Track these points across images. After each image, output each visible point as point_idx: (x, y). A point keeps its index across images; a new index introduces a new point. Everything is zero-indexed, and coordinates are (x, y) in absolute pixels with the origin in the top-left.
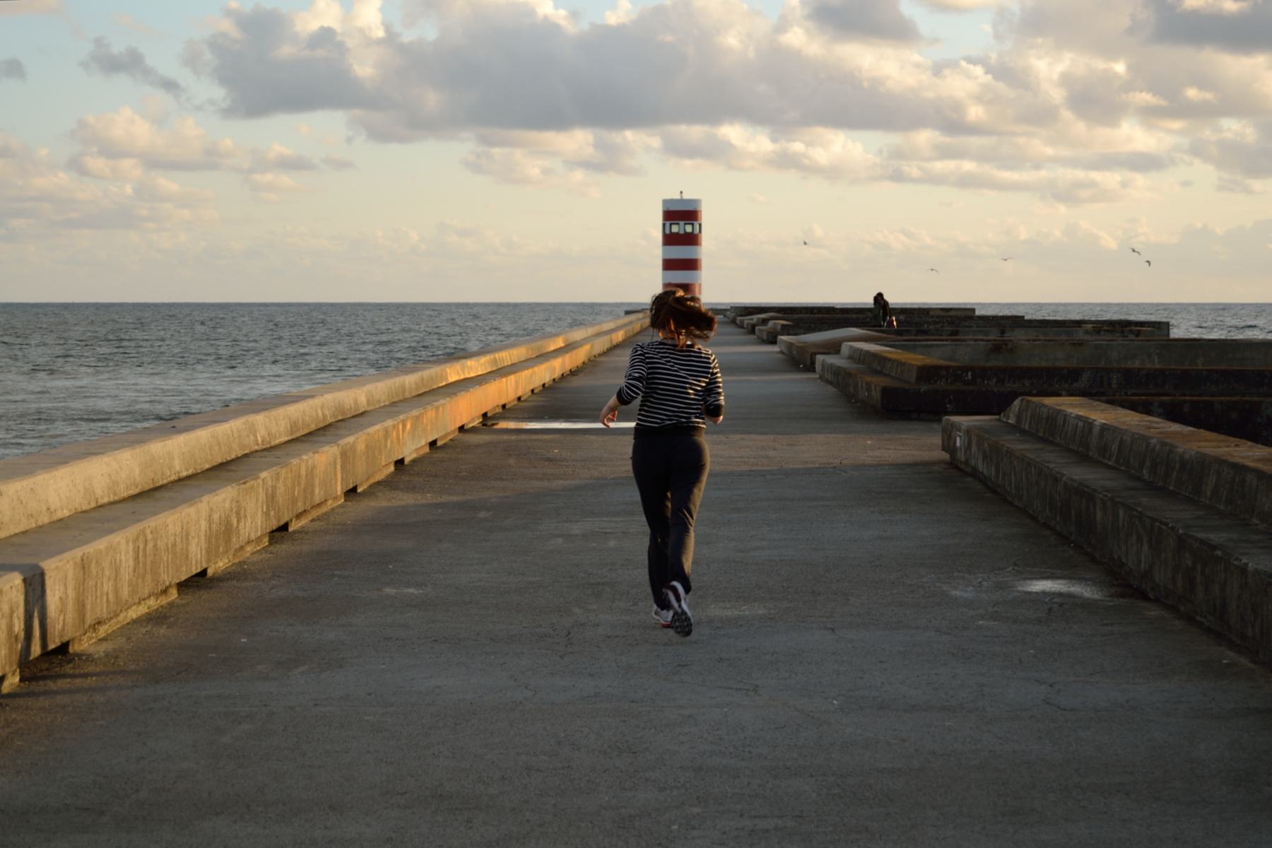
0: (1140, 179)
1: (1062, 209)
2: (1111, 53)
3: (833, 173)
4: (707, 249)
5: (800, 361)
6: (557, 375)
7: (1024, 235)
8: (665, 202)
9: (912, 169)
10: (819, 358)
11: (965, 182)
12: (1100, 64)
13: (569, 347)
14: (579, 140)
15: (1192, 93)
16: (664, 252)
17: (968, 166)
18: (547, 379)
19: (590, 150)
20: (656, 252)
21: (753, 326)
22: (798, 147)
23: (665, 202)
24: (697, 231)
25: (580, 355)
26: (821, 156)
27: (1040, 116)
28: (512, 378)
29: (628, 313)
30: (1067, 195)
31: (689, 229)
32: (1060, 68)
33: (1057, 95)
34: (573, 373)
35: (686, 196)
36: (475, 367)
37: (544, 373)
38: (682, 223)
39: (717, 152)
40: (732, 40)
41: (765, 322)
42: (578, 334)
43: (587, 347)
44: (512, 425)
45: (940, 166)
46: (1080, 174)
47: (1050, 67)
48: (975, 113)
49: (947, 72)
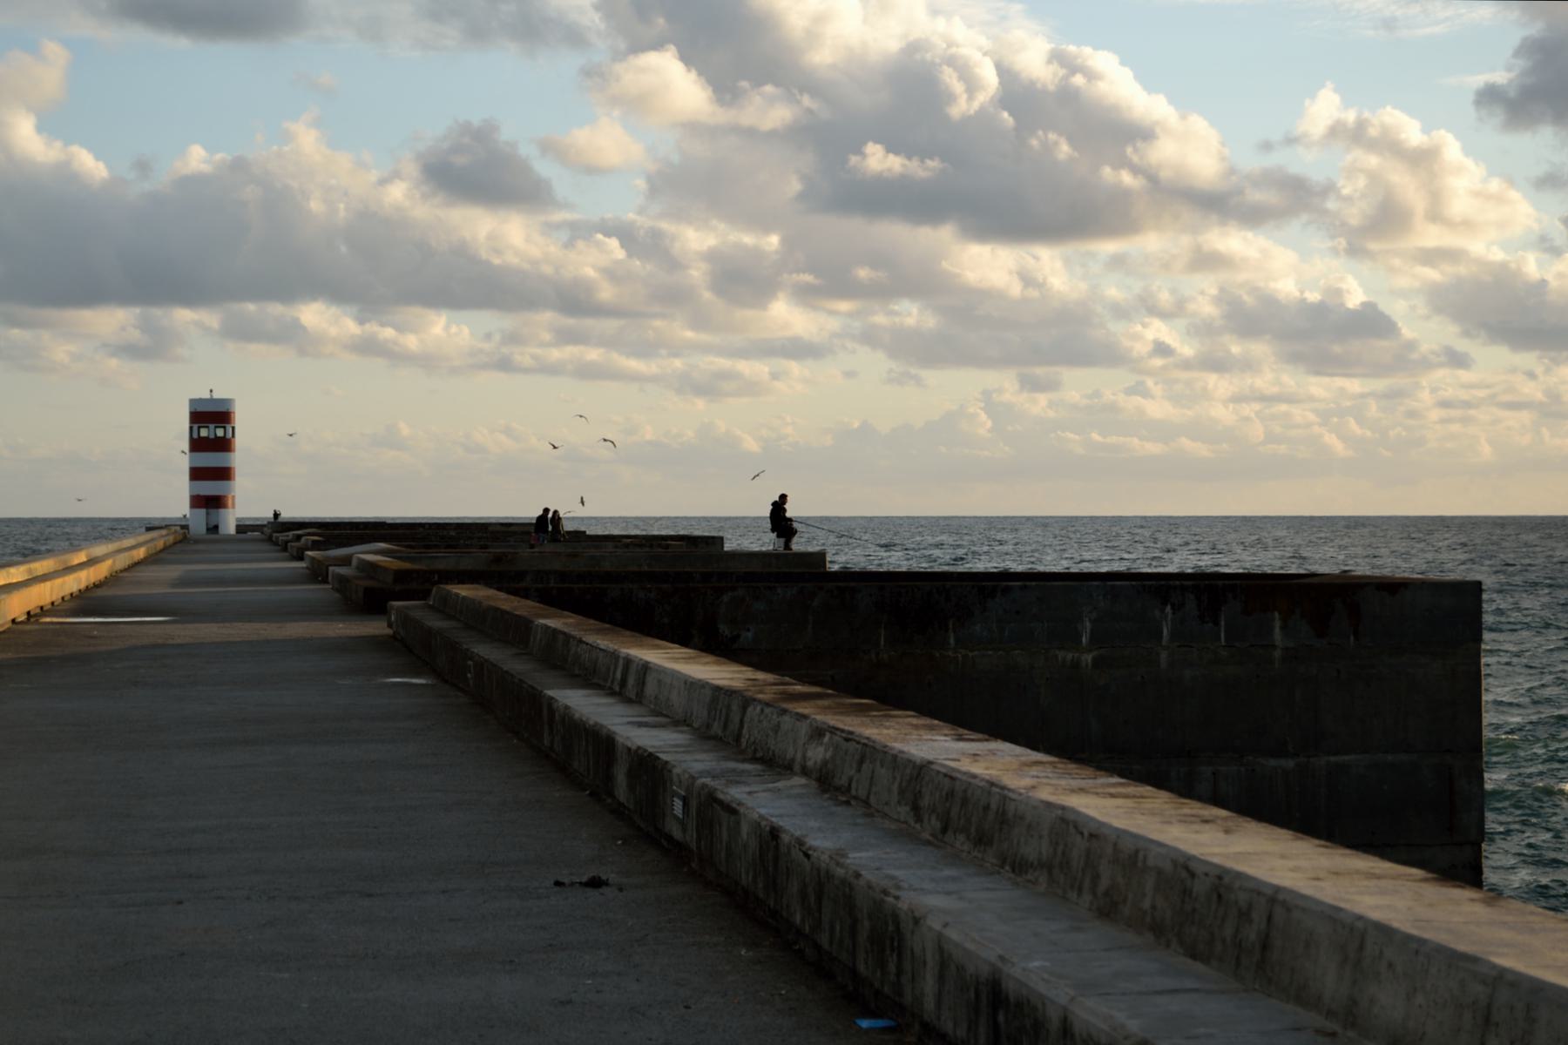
0: (794, 367)
1: (700, 403)
2: (763, 223)
3: (427, 361)
4: (238, 460)
5: (318, 574)
6: (82, 586)
7: (649, 434)
8: (192, 401)
11: (587, 372)
12: (748, 239)
13: (91, 562)
14: (113, 320)
15: (863, 273)
16: (191, 460)
17: (593, 355)
20: (182, 461)
23: (192, 401)
24: (229, 435)
26: (411, 342)
27: (673, 298)
28: (48, 584)
30: (709, 388)
31: (220, 433)
33: (697, 274)
34: (97, 586)
35: (216, 396)
38: (212, 426)
39: (291, 335)
40: (315, 205)
41: (298, 538)
42: (99, 550)
43: (109, 562)
45: (556, 354)
46: (724, 363)
47: (697, 239)
48: (606, 293)
49: (580, 244)
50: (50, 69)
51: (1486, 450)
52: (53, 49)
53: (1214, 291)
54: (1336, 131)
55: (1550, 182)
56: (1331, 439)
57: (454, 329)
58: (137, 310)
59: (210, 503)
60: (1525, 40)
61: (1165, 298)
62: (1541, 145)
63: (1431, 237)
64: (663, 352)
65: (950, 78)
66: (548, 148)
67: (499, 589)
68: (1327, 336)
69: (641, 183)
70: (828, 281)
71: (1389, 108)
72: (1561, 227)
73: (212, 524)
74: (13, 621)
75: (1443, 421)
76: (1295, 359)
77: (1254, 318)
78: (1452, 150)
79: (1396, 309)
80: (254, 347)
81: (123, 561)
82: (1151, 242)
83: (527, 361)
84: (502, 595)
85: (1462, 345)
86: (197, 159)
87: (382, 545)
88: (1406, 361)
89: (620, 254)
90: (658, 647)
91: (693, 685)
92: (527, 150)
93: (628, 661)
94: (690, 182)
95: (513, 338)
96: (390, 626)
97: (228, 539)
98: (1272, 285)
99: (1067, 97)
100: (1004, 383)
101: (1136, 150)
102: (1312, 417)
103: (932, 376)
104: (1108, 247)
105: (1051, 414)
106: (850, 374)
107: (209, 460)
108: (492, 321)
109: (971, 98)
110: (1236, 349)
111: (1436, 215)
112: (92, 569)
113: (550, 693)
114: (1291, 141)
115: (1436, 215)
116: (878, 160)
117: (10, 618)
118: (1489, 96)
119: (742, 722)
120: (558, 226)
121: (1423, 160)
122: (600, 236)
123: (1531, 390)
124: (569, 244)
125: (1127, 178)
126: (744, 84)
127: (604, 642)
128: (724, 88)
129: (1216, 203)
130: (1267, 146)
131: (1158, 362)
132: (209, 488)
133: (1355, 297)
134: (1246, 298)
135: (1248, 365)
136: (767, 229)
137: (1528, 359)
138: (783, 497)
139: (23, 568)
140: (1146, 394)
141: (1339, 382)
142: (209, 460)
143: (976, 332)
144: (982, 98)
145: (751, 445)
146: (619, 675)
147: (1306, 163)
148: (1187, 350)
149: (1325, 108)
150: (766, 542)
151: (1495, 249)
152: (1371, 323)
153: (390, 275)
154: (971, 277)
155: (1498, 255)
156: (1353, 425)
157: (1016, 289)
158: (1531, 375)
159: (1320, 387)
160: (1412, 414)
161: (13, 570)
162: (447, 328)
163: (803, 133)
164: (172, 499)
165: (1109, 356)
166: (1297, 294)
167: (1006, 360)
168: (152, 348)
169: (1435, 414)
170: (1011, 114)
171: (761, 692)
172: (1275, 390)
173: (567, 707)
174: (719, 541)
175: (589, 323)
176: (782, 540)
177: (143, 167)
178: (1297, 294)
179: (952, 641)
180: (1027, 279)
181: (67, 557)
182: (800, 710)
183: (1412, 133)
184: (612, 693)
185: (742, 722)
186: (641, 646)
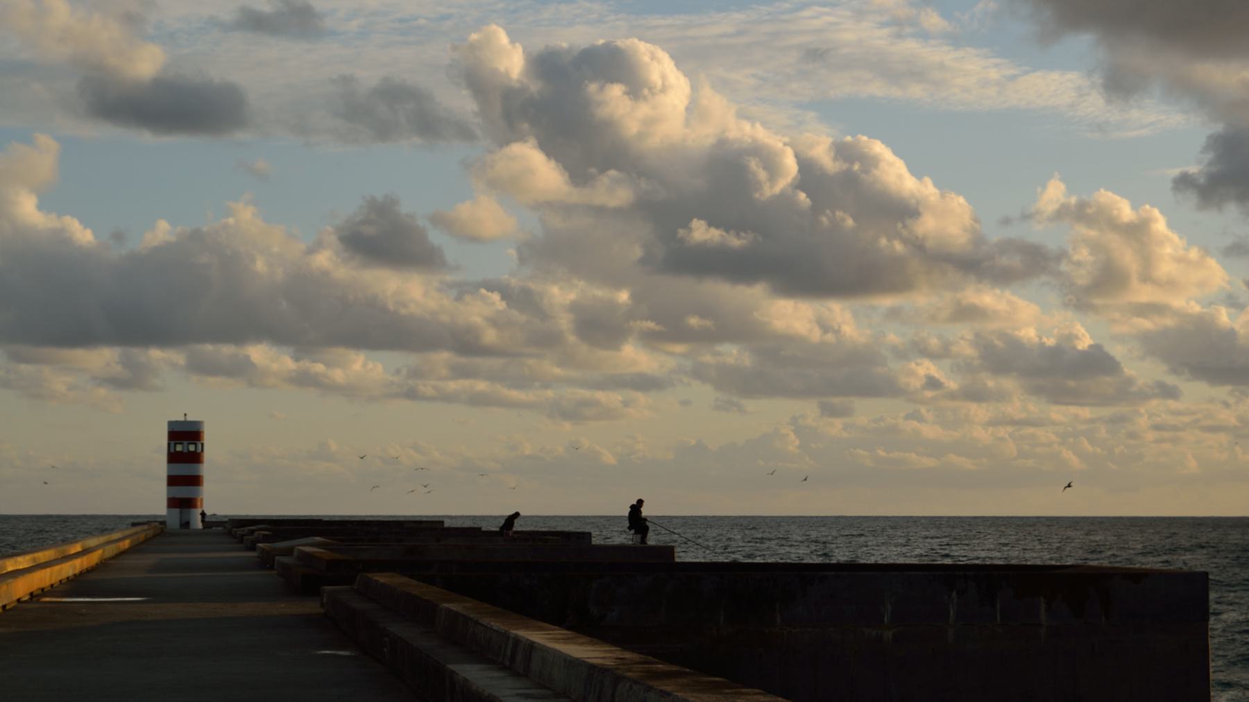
0: (640, 396)
1: (567, 426)
2: (616, 281)
3: (349, 391)
4: (209, 469)
5: (266, 562)
6: (77, 571)
7: (528, 450)
8: (171, 423)
9: (426, 388)
10: (277, 558)
11: (477, 400)
12: (600, 293)
13: (86, 552)
14: (103, 358)
15: (694, 321)
16: (169, 469)
17: (481, 386)
18: (70, 573)
19: (119, 368)
21: (243, 536)
22: (319, 368)
23: (171, 423)
25: (94, 558)
26: (338, 375)
27: (547, 340)
28: (48, 570)
29: (134, 525)
30: (573, 413)
31: (192, 448)
32: (572, 296)
33: (564, 322)
34: (90, 571)
35: (189, 419)
36: (23, 562)
37: (77, 566)
38: (185, 443)
39: (241, 370)
40: (260, 266)
41: (252, 532)
42: (92, 542)
43: (100, 551)
44: (48, 599)
45: (452, 386)
47: (562, 294)
48: (490, 336)
49: (468, 298)
50: (44, 156)
51: (1193, 464)
52: (44, 139)
53: (970, 336)
54: (1062, 213)
55: (1236, 251)
56: (1068, 455)
57: (370, 365)
59: (183, 504)
60: (1210, 137)
61: (934, 342)
62: (1230, 220)
63: (1144, 294)
64: (537, 384)
65: (754, 164)
66: (438, 220)
67: (411, 577)
68: (1065, 373)
69: (512, 253)
70: (669, 329)
71: (1102, 191)
72: (1244, 288)
74: (19, 600)
75: (1158, 441)
76: (1037, 391)
77: (1004, 357)
78: (1160, 225)
79: (1117, 351)
80: (211, 380)
81: (110, 551)
82: (921, 300)
83: (429, 391)
84: (414, 582)
85: (1171, 380)
86: (163, 231)
87: (318, 539)
88: (1126, 393)
89: (501, 305)
90: (541, 629)
91: (572, 664)
92: (421, 223)
93: (517, 641)
94: (552, 251)
95: (416, 373)
96: (322, 606)
97: (197, 533)
98: (1017, 332)
99: (850, 182)
100: (808, 410)
101: (905, 226)
102: (1054, 438)
103: (751, 405)
104: (886, 302)
105: (845, 435)
106: (685, 403)
107: (183, 469)
108: (402, 360)
109: (772, 187)
110: (991, 384)
111: (1146, 278)
112: (85, 558)
113: (451, 667)
114: (1027, 217)
115: (1146, 278)
116: (701, 232)
117: (15, 598)
118: (1184, 182)
119: (613, 696)
120: (451, 286)
121: (1137, 232)
122: (483, 291)
123: (1228, 417)
124: (459, 298)
125: (898, 247)
126: (593, 170)
127: (496, 625)
128: (578, 175)
129: (973, 263)
130: (1006, 221)
131: (929, 394)
132: (182, 492)
133: (1085, 342)
134: (996, 342)
135: (1001, 396)
136: (618, 284)
137: (1222, 392)
138: (640, 502)
139: (28, 557)
140: (921, 419)
141: (1073, 410)
142: (183, 469)
143: (784, 370)
144: (782, 184)
145: (609, 458)
146: (509, 652)
147: (1036, 233)
148: (952, 384)
149: (1054, 194)
150: (622, 537)
151: (1193, 303)
152: (1097, 362)
153: (318, 322)
154: (779, 325)
155: (1196, 309)
156: (1087, 446)
157: (816, 335)
158: (1226, 405)
159: (1059, 413)
160: (1132, 435)
161: (20, 559)
162: (364, 365)
163: (646, 208)
164: (153, 500)
165: (886, 388)
166: (1037, 340)
167: (806, 392)
168: (132, 380)
169: (1151, 436)
170: (808, 196)
171: (630, 671)
172: (1023, 415)
173: (466, 680)
175: (479, 361)
176: (639, 536)
177: (118, 237)
178: (1037, 340)
179: (779, 620)
180: (825, 327)
181: (65, 547)
182: (663, 688)
183: (1126, 211)
184: (503, 668)
185: (613, 696)
186: (527, 628)
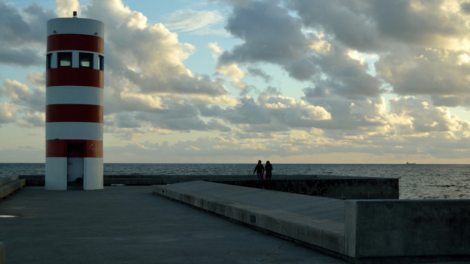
24: (97, 66)
58: (45, 96)
59: (74, 150)
73: (73, 179)
132: (72, 131)
174: (393, 184)
